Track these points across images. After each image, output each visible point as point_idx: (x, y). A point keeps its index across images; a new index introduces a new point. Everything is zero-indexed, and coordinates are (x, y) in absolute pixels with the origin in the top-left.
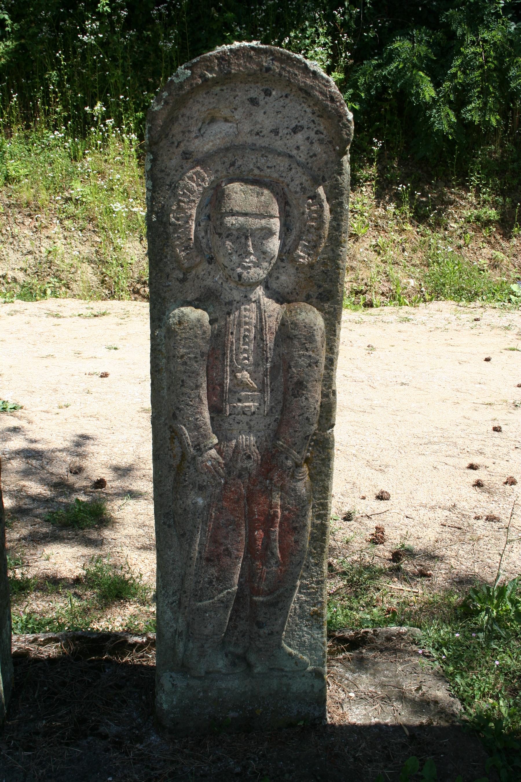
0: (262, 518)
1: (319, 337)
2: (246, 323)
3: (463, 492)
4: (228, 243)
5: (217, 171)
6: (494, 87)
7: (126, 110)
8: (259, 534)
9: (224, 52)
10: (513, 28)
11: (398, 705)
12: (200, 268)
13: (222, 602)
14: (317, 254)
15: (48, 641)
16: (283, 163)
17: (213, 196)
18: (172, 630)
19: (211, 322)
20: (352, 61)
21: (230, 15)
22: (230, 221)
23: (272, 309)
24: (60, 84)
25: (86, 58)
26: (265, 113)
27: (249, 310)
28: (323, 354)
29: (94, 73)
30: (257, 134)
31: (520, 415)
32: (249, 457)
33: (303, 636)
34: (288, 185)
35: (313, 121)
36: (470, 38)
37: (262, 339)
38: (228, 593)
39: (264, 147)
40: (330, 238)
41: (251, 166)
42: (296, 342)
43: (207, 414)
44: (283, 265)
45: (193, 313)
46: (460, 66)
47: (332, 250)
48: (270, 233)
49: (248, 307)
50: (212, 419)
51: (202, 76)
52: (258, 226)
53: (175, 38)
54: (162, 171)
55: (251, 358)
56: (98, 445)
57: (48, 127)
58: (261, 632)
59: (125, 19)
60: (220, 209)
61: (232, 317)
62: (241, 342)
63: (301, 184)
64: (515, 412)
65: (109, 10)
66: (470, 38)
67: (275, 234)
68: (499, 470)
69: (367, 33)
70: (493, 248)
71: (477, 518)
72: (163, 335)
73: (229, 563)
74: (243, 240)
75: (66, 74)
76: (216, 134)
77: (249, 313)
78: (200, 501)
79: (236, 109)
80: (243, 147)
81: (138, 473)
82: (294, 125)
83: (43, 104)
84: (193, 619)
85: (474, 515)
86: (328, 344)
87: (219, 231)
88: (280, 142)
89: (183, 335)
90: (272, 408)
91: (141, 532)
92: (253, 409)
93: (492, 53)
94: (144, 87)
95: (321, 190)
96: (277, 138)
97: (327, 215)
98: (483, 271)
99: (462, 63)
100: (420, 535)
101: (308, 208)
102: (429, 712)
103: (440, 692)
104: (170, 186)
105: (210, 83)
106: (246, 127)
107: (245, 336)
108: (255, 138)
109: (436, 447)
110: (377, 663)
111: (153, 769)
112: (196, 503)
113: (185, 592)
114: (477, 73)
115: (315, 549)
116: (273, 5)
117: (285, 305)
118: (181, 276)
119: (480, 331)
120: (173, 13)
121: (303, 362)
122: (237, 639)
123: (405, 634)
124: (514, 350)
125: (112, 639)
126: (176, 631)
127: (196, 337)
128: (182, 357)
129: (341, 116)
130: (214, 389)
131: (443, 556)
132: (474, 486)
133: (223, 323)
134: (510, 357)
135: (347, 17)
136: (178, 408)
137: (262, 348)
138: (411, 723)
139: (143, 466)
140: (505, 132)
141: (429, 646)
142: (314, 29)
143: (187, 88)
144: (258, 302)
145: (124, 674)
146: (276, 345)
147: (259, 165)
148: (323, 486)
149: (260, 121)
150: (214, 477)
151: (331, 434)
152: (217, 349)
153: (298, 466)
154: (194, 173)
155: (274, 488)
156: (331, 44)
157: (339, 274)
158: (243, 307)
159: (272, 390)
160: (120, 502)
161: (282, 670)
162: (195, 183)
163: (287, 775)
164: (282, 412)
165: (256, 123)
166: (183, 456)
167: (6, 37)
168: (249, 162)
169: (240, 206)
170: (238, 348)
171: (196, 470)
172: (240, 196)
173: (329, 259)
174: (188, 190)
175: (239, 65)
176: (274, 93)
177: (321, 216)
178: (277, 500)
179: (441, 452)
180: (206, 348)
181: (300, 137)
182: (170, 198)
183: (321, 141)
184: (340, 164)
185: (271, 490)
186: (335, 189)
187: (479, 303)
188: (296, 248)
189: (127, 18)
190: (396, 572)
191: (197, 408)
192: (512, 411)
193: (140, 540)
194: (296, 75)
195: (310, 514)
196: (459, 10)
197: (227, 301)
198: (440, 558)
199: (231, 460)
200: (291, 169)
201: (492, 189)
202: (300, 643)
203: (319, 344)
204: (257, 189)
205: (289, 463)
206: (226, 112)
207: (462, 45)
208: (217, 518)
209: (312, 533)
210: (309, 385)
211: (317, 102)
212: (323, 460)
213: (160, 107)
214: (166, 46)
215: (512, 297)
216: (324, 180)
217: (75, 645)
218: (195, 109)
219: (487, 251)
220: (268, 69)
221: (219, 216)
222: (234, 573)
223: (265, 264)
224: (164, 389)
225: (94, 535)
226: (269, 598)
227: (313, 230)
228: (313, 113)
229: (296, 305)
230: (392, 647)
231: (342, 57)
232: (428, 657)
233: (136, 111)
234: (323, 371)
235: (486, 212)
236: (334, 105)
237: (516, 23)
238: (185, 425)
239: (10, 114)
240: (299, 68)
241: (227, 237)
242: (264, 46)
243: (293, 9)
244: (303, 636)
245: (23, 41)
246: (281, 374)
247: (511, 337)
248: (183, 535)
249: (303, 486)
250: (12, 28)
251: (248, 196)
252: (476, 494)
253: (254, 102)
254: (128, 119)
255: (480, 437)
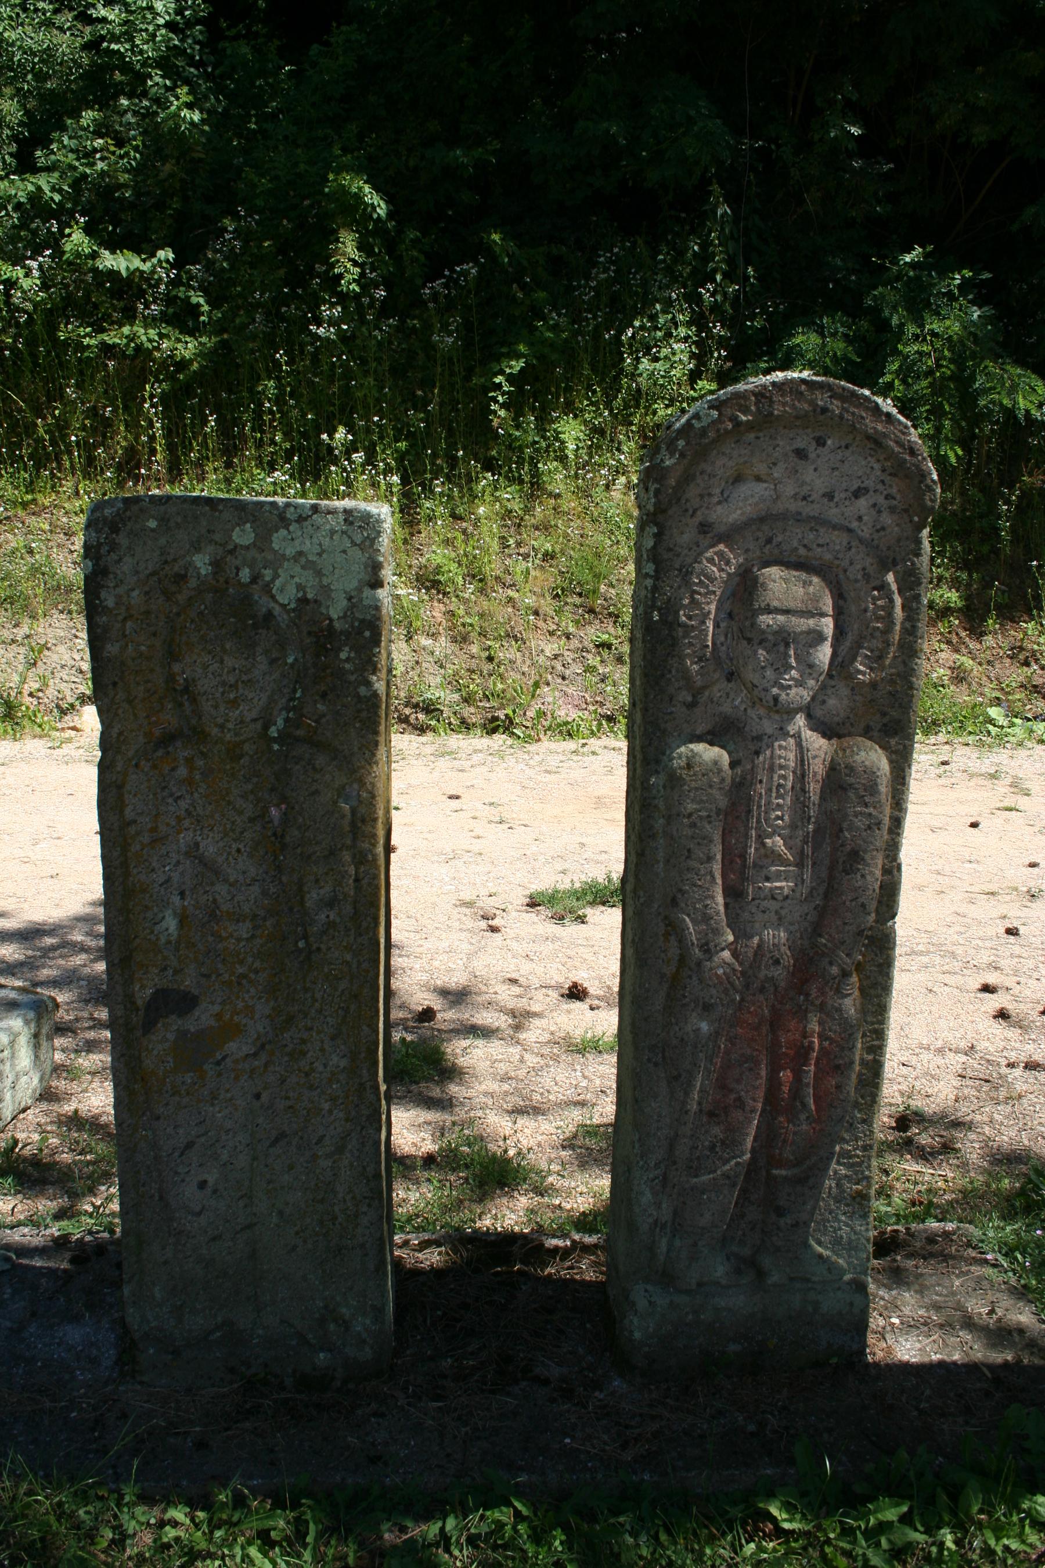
0: (792, 1052)
1: (884, 788)
2: (781, 767)
3: (980, 1027)
4: (760, 651)
5: (747, 551)
6: (951, 405)
7: (382, 438)
8: (786, 1075)
9: (764, 386)
10: (975, 315)
11: (966, 1336)
12: (715, 689)
13: (728, 1177)
14: (882, 668)
15: (424, 1245)
16: (839, 540)
17: (738, 585)
18: (650, 1220)
19: (733, 765)
20: (729, 364)
21: (542, 295)
22: (766, 620)
23: (817, 746)
24: (279, 400)
25: (318, 360)
26: (815, 470)
27: (785, 748)
28: (887, 811)
29: (333, 382)
30: (804, 498)
31: (1044, 912)
32: (777, 962)
33: (840, 1229)
34: (845, 571)
35: (883, 482)
36: (911, 329)
37: (803, 790)
38: (738, 1164)
39: (814, 517)
40: (901, 645)
41: (795, 544)
42: (851, 794)
43: (720, 899)
44: (833, 683)
45: (708, 753)
46: (897, 373)
47: (904, 662)
48: (818, 638)
49: (784, 743)
50: (726, 905)
51: (733, 419)
52: (804, 628)
53: (457, 330)
54: (670, 550)
55: (786, 818)
56: (408, 956)
57: (260, 465)
58: (782, 1222)
59: (382, 302)
60: (751, 604)
61: (761, 758)
62: (774, 795)
63: (864, 569)
64: (1033, 905)
65: (357, 289)
66: (911, 329)
67: (826, 639)
68: (1028, 992)
69: (752, 321)
70: (957, 651)
71: (1011, 1065)
72: (661, 783)
73: (741, 1119)
74: (782, 649)
75: (289, 384)
76: (746, 499)
77: (786, 753)
78: (704, 1026)
79: (775, 464)
80: (784, 516)
81: (480, 999)
82: (855, 487)
83: (253, 430)
84: (684, 1203)
85: (1004, 1062)
86: (893, 797)
87: (749, 635)
88: (834, 511)
89: (693, 784)
90: (813, 889)
91: (506, 1087)
92: (786, 891)
93: (946, 353)
94: (409, 404)
95: (890, 577)
96: (832, 504)
97: (898, 613)
98: (943, 686)
99: (900, 367)
100: (930, 1091)
101: (872, 603)
102: (1012, 1345)
103: (1024, 1316)
104: (680, 570)
105: (742, 428)
106: (789, 489)
107: (779, 786)
108: (800, 504)
109: (925, 959)
110: (922, 1275)
111: (627, 1427)
112: (699, 1029)
113: (675, 1163)
114: (924, 383)
115: (862, 1097)
116: (606, 280)
117: (834, 741)
118: (690, 699)
119: (953, 780)
120: (454, 292)
121: (860, 823)
122: (744, 1235)
123: (954, 1233)
124: (1011, 810)
125: (520, 1242)
126: (656, 1222)
127: (711, 786)
128: (690, 815)
129: (924, 475)
130: (732, 862)
131: (971, 1122)
132: (995, 1017)
133: (749, 767)
134: (1007, 820)
135: (719, 298)
136: (680, 890)
137: (803, 803)
138: (991, 1361)
139: (484, 988)
140: (967, 471)
141: (994, 1251)
142: (670, 316)
143: (711, 434)
144: (797, 736)
145: (550, 1293)
146: (822, 798)
147: (806, 542)
148: (879, 1005)
149: (808, 480)
150: (726, 991)
151: (893, 928)
152: (739, 802)
153: (845, 974)
154: (716, 553)
155: (811, 1008)
156: (695, 339)
157: (913, 696)
158: (776, 744)
159: (814, 864)
160: (465, 1043)
161: (808, 1280)
162: (717, 566)
163: (825, 1436)
164: (826, 896)
165: (804, 483)
166: (682, 960)
167: (199, 331)
168: (793, 538)
169: (779, 600)
170: (769, 803)
171: (701, 981)
172: (780, 584)
173: (898, 675)
174: (707, 576)
175: (784, 404)
176: (829, 442)
177: (890, 614)
178: (814, 1026)
179: (934, 966)
180: (723, 802)
181: (863, 503)
182: (679, 587)
183: (892, 510)
184: (918, 542)
185: (806, 1011)
186: (910, 575)
187: (942, 737)
188: (854, 659)
189: (384, 301)
190: (907, 1146)
191: (708, 889)
192: (1029, 904)
193: (508, 1099)
194: (862, 418)
195: (859, 1046)
196: (893, 288)
197: (754, 734)
198: (969, 1126)
199: (751, 967)
200: (850, 548)
201: (950, 559)
202: (833, 1241)
203: (883, 797)
204: (804, 575)
205: (835, 970)
206: (761, 468)
207: (899, 341)
208: (727, 1052)
209: (860, 1074)
210: (867, 857)
211: (891, 455)
212: (880, 965)
213: (673, 461)
214: (442, 342)
215: (990, 727)
216: (895, 563)
217: (467, 1250)
218: (719, 463)
219: (946, 655)
220: (824, 410)
221: (750, 614)
222: (747, 1134)
223: (811, 683)
224: (658, 862)
225: (436, 1092)
226: (796, 1171)
227: (878, 634)
228: (884, 471)
229: (848, 741)
230: (938, 1251)
231: (712, 357)
232: (994, 1266)
233: (397, 441)
234: (886, 837)
235: (942, 596)
236: (914, 460)
237: (980, 308)
238: (689, 915)
239: (204, 445)
240: (867, 409)
241: (760, 643)
242: (818, 379)
243: (637, 286)
244: (840, 1229)
245: (225, 336)
246: (828, 841)
247: (1003, 790)
248: (676, 1078)
249: (850, 1005)
250: (210, 318)
251: (791, 585)
252: (999, 1029)
253: (801, 454)
254: (383, 451)
255: (988, 944)
